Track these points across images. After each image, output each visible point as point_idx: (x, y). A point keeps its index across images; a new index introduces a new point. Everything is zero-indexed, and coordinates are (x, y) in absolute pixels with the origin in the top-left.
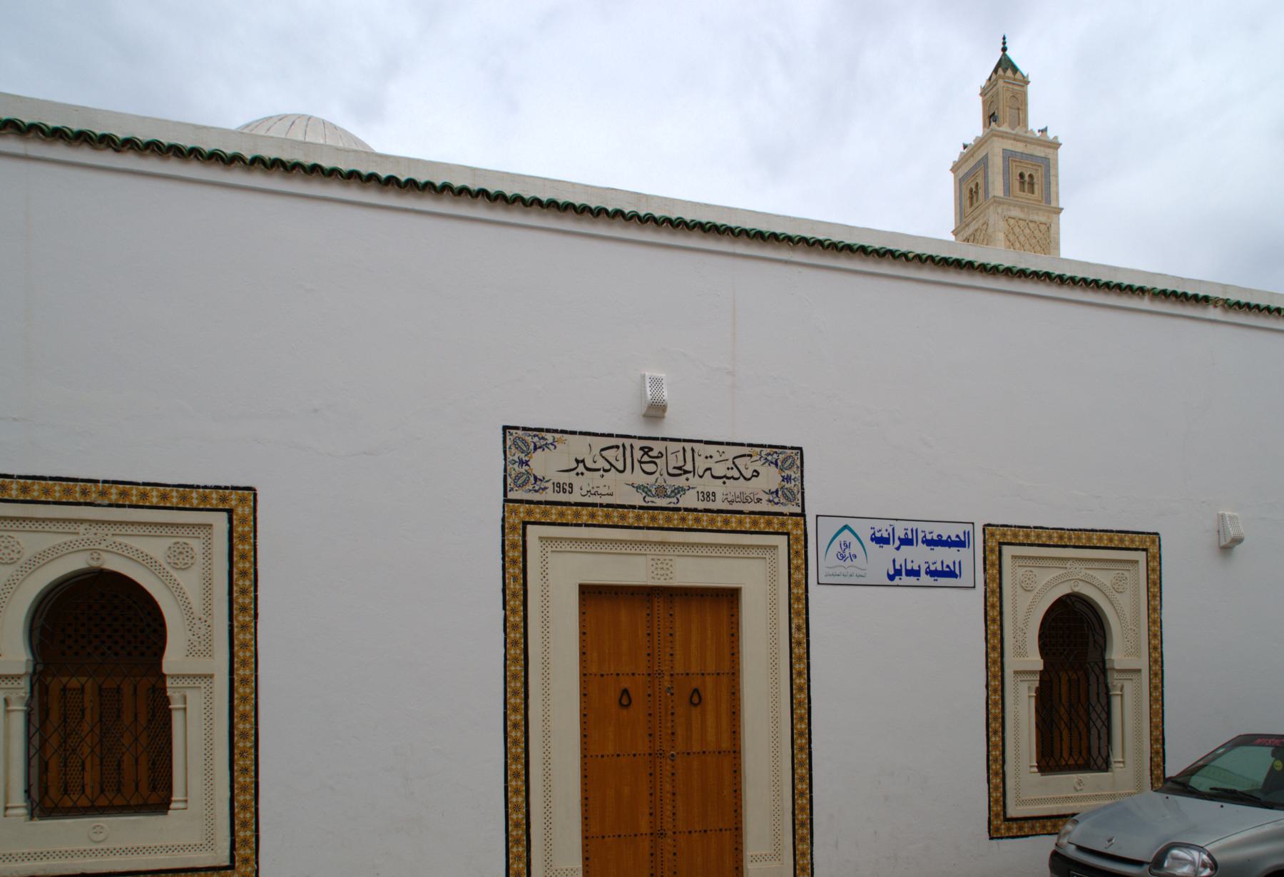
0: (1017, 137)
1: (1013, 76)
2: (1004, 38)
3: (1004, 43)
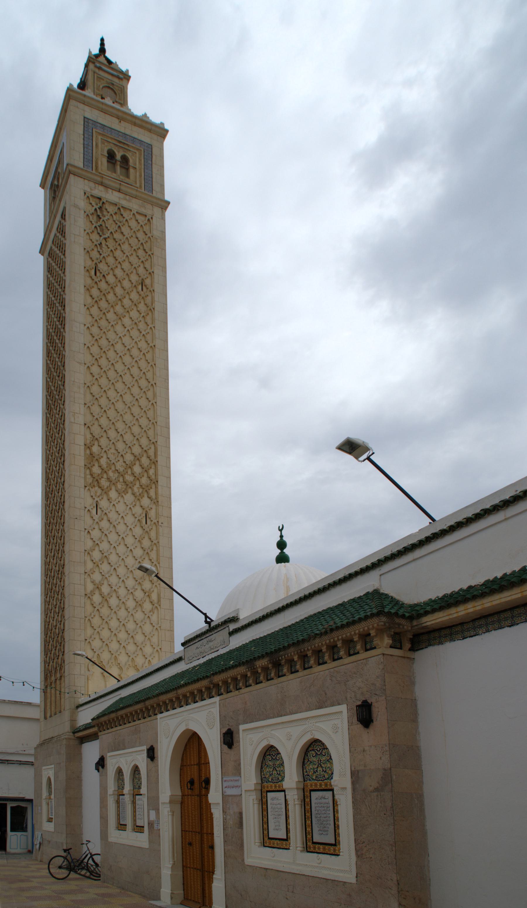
2: (102, 40)
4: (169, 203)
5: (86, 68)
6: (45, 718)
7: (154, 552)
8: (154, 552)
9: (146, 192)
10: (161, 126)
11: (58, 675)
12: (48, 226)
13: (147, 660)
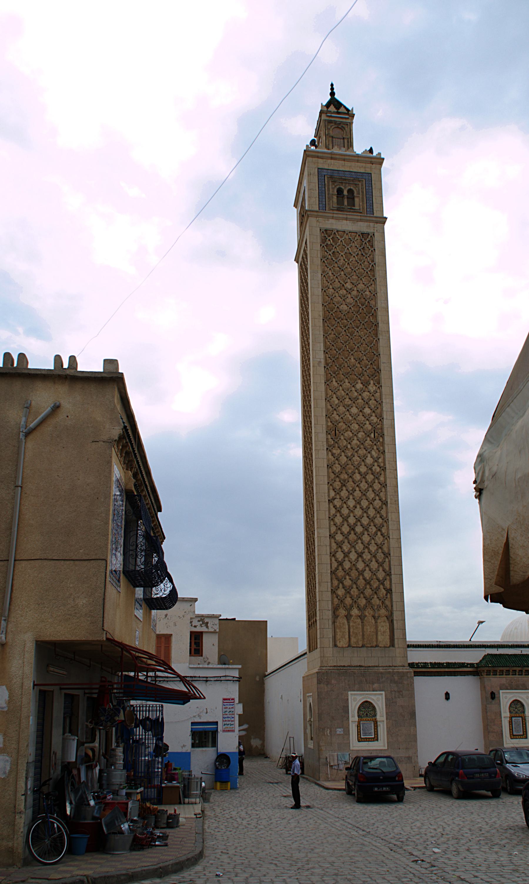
0: (333, 156)
1: (336, 111)
2: (332, 85)
3: (332, 89)
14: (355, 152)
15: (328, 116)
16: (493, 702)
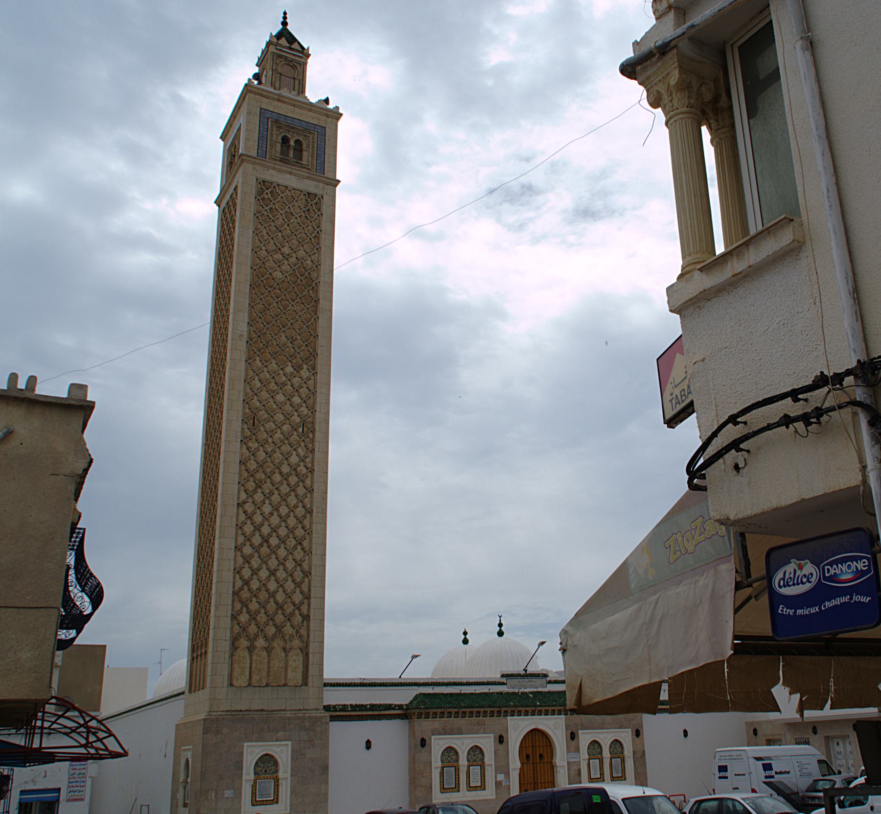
2: (285, 13)
3: (285, 18)
4: (341, 115)
5: (267, 49)
6: (190, 691)
7: (308, 540)
8: (309, 478)
9: (317, 174)
10: (336, 110)
11: (203, 651)
12: (224, 186)
13: (295, 630)
14: (309, 100)
15: (277, 49)
16: (424, 750)
